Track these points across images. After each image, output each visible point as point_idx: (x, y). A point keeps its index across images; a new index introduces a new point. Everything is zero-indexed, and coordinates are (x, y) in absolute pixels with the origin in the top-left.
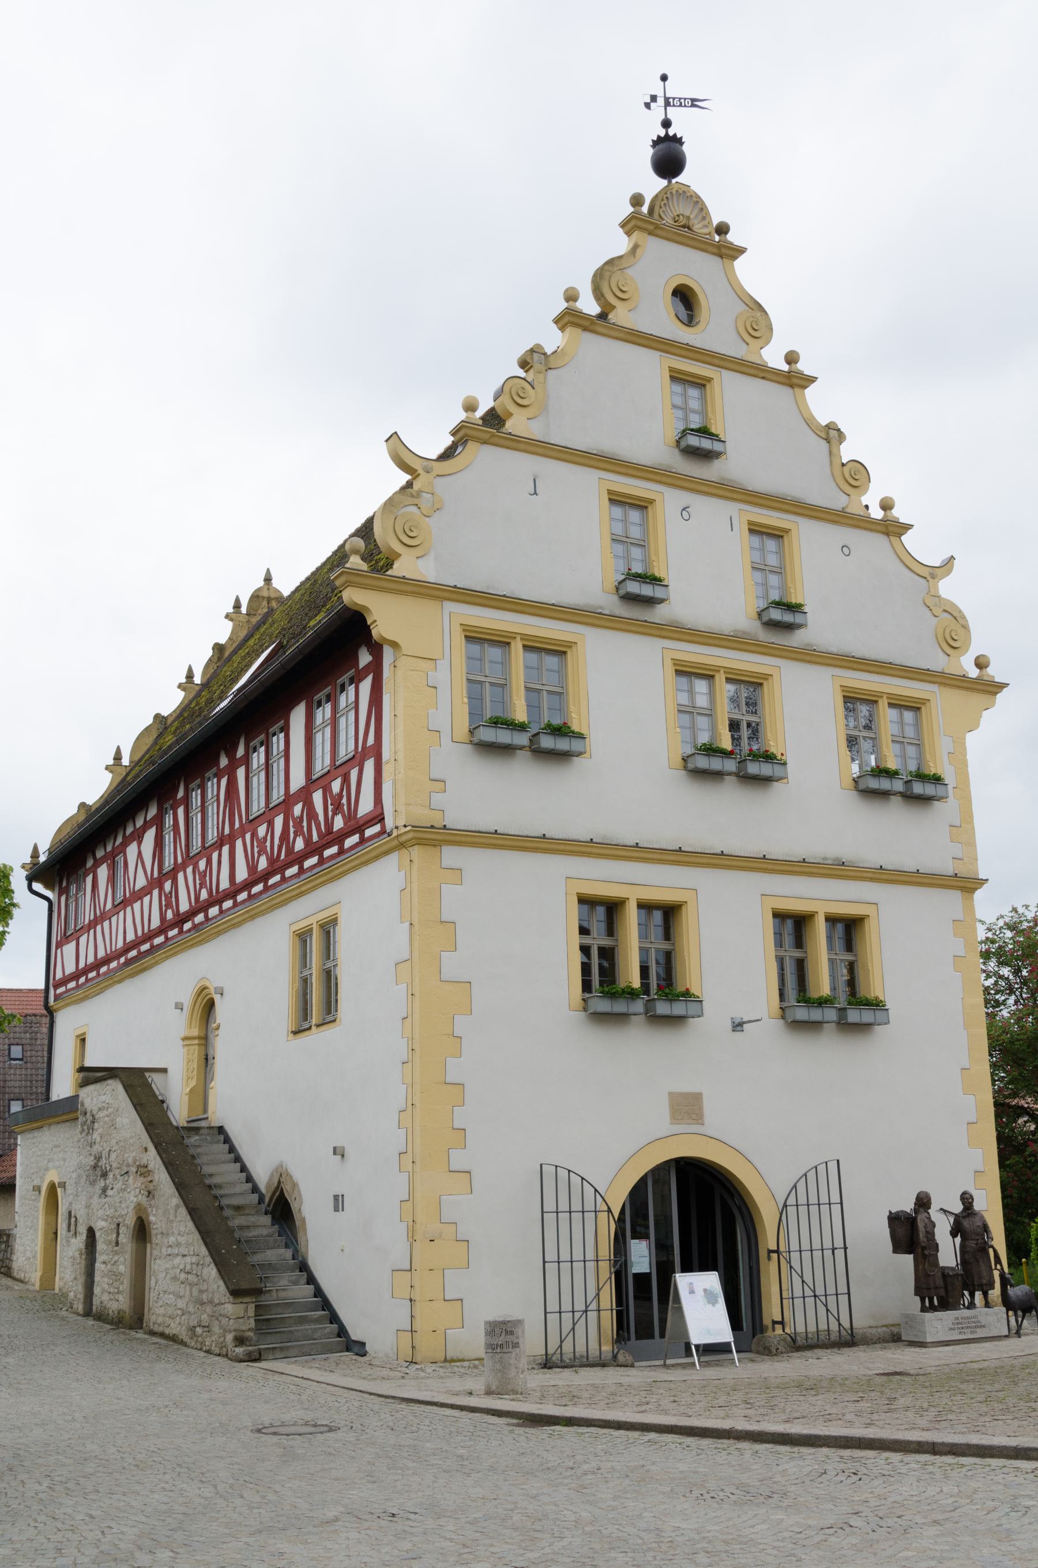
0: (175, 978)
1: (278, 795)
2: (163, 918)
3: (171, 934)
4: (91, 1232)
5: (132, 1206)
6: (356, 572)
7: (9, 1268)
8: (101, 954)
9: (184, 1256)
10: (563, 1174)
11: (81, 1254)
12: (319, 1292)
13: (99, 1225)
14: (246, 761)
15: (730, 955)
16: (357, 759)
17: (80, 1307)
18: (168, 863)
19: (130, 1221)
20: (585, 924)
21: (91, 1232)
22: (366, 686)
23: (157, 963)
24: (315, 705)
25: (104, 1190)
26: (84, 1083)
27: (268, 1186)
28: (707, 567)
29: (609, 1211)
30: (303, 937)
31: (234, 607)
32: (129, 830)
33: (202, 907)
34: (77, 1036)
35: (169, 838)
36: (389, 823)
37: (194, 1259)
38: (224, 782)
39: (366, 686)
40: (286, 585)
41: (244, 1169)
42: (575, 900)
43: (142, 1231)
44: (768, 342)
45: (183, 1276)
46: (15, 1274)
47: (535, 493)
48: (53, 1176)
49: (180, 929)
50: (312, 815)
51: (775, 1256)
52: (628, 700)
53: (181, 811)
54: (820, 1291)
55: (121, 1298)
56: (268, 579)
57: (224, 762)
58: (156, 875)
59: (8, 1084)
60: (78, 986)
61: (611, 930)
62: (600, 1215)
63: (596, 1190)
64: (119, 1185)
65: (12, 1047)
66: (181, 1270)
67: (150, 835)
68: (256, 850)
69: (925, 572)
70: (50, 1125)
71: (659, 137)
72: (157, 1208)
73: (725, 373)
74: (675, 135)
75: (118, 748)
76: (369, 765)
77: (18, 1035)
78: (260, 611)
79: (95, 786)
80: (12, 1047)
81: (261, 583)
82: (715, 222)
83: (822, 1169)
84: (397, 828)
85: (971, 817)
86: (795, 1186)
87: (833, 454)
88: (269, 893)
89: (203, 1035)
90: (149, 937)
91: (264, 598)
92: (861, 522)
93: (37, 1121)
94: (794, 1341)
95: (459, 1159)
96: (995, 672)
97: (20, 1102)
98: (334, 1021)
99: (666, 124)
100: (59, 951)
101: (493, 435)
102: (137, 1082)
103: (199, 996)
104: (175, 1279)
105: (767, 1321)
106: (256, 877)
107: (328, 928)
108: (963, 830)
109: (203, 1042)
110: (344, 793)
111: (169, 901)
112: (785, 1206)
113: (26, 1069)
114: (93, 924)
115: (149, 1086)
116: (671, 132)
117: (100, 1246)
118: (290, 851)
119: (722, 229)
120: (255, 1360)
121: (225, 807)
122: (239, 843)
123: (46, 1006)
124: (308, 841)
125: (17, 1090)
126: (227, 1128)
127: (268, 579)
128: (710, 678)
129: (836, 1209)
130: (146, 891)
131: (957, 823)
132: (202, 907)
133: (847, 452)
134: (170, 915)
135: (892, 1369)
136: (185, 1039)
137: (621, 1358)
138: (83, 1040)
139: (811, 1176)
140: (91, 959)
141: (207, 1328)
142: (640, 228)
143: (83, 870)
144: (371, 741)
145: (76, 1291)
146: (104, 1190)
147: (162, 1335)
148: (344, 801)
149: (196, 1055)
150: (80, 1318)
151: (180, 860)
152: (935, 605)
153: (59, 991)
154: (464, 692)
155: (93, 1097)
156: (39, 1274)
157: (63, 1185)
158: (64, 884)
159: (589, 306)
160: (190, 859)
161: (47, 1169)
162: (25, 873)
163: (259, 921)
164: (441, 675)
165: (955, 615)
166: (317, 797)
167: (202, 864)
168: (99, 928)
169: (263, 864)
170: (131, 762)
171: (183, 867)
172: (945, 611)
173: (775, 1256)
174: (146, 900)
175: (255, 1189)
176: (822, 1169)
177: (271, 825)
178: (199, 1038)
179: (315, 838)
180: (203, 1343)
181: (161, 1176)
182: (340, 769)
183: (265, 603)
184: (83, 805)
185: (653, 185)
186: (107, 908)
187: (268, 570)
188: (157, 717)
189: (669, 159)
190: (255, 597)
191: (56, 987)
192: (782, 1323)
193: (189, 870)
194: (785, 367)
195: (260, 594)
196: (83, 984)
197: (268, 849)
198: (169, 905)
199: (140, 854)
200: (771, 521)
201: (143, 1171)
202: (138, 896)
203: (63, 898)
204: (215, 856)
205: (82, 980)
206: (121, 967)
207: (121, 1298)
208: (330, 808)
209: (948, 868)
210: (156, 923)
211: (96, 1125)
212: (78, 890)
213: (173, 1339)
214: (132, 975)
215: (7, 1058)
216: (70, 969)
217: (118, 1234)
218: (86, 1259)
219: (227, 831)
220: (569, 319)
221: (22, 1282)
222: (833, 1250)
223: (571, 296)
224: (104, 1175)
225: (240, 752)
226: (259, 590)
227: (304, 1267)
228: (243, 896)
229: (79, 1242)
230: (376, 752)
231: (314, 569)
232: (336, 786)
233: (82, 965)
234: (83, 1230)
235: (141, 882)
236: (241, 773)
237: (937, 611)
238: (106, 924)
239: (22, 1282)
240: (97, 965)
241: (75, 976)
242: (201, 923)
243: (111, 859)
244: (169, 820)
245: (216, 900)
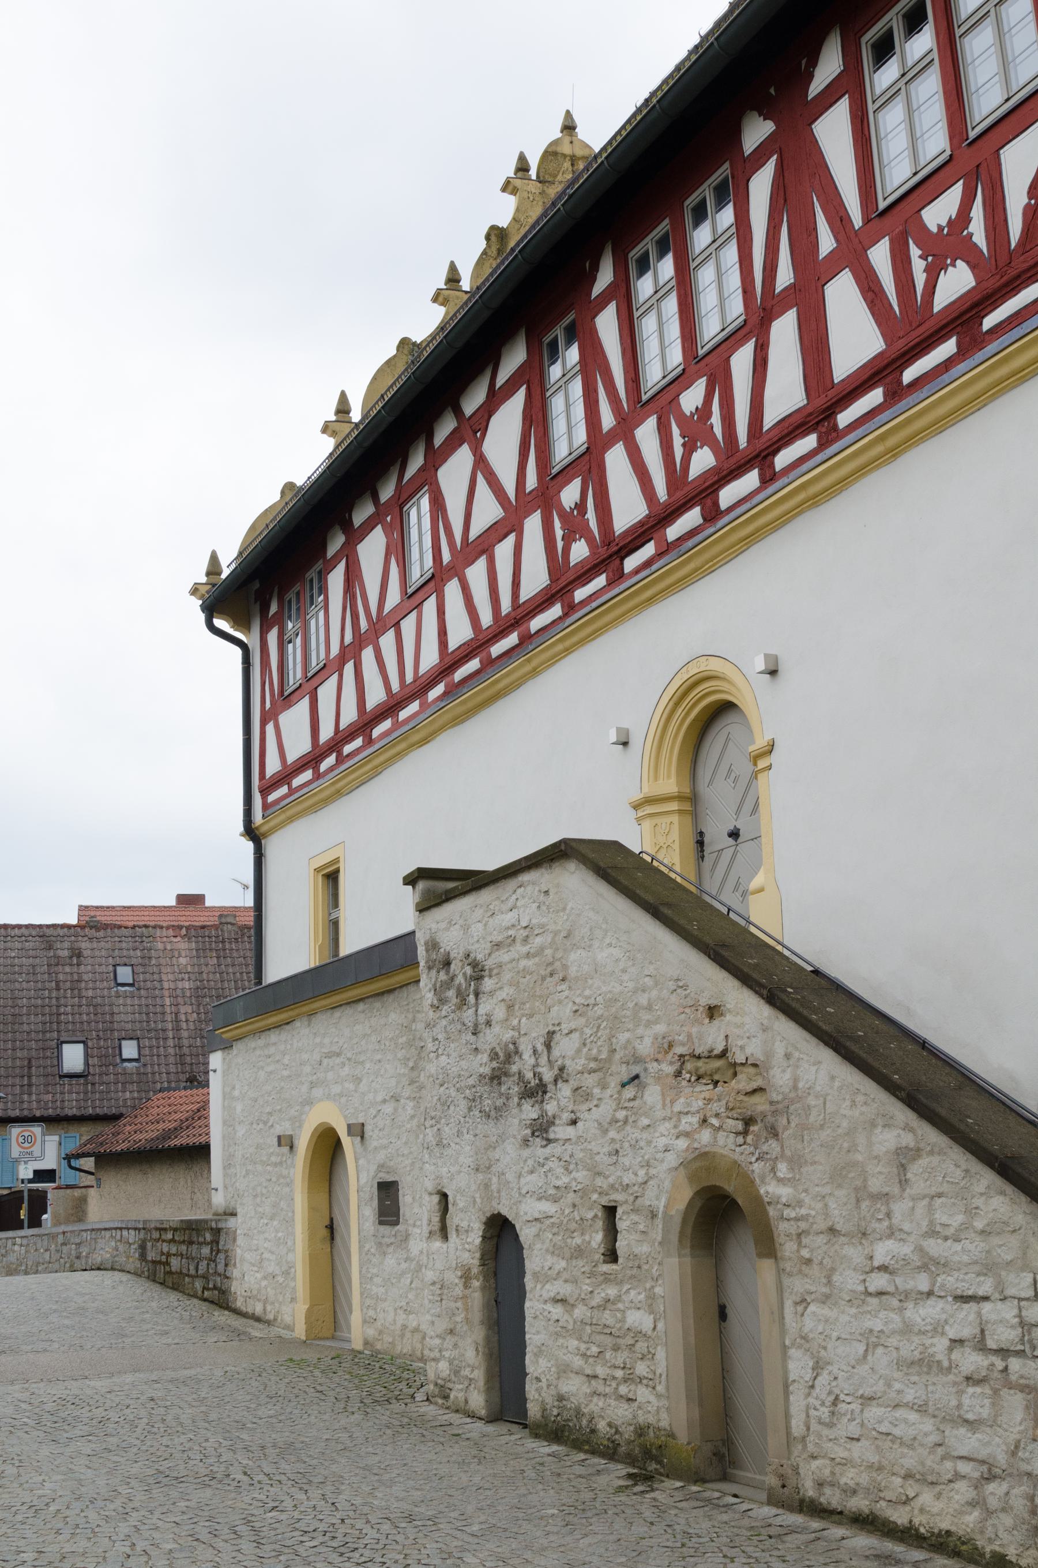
4: (500, 1231)
7: (224, 1292)
11: (466, 1277)
13: (526, 1213)
21: (500, 1231)
23: (534, 673)
25: (541, 1129)
34: (317, 870)
40: (598, 133)
46: (239, 1304)
48: (329, 1113)
55: (643, 1393)
56: (569, 127)
59: (117, 1018)
65: (119, 969)
70: (311, 1014)
72: (796, 1162)
75: (343, 394)
77: (125, 953)
78: (559, 178)
80: (119, 969)
81: (557, 134)
89: (687, 790)
91: (565, 156)
93: (279, 1009)
97: (134, 1043)
100: (270, 728)
103: (677, 704)
109: (687, 806)
113: (140, 997)
123: (251, 832)
125: (129, 1026)
127: (569, 127)
130: (510, 525)
138: (332, 877)
140: (350, 715)
143: (319, 565)
145: (459, 1357)
146: (541, 1129)
149: (675, 835)
150: (480, 1424)
153: (271, 798)
156: (302, 1308)
157: (358, 1131)
161: (309, 1102)
163: (1026, 384)
178: (680, 798)
183: (567, 164)
184: (289, 486)
186: (388, 607)
188: (404, 342)
190: (550, 154)
191: (265, 791)
195: (559, 149)
201: (714, 1067)
203: (273, 637)
211: (488, 984)
214: (458, 720)
215: (112, 984)
218: (483, 1288)
221: (258, 1320)
226: (556, 143)
231: (647, 95)
233: (326, 733)
235: (487, 511)
238: (387, 641)
239: (258, 1320)
241: (311, 761)
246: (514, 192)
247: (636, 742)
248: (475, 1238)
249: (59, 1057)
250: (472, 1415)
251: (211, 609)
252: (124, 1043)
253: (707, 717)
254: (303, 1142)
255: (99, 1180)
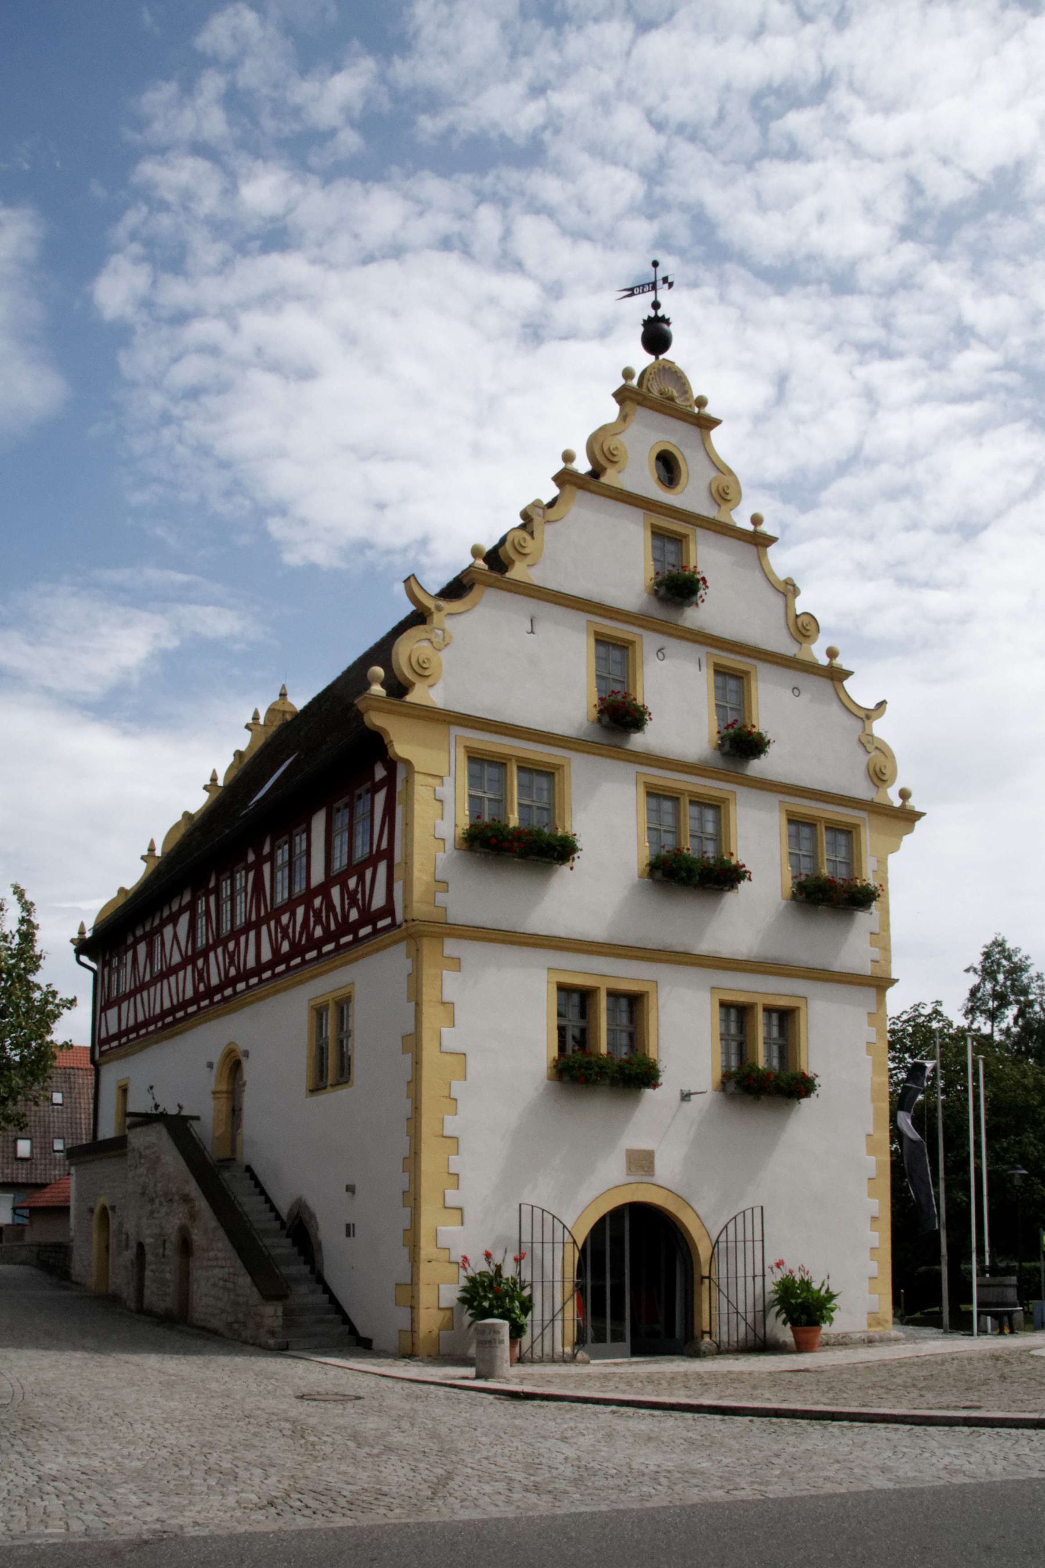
0: (207, 1041)
1: (299, 888)
2: (195, 989)
3: (203, 1004)
4: (141, 1246)
5: (176, 1227)
6: (376, 698)
8: (141, 1018)
9: (223, 1267)
10: (538, 1213)
11: (132, 1264)
12: (333, 1300)
13: (148, 1241)
14: (271, 857)
15: (686, 1036)
16: (372, 861)
17: (132, 1305)
18: (201, 942)
19: (174, 1238)
20: (562, 1010)
21: (141, 1246)
22: (380, 798)
24: (334, 811)
25: (152, 1212)
26: (132, 1126)
27: (289, 1214)
28: (680, 709)
29: (574, 1242)
30: (319, 1012)
31: (254, 719)
32: (166, 913)
33: (232, 982)
34: (120, 1087)
35: (201, 923)
36: (399, 917)
37: (231, 1270)
38: (251, 875)
39: (380, 798)
40: (299, 702)
41: (268, 1200)
42: (554, 988)
43: (186, 1247)
44: (738, 504)
45: (221, 1283)
47: (532, 632)
48: (103, 1200)
49: (211, 1001)
50: (330, 907)
51: (707, 1281)
52: (609, 821)
53: (212, 899)
54: (741, 1309)
56: (283, 695)
57: (251, 857)
58: (190, 953)
60: (120, 1045)
61: (583, 1014)
62: (567, 1246)
63: (564, 1226)
64: (164, 1210)
66: (218, 1276)
67: (184, 920)
68: (279, 935)
69: (862, 714)
71: (649, 317)
73: (699, 531)
74: (663, 316)
76: (382, 867)
79: (132, 874)
81: (277, 698)
82: (695, 395)
83: (749, 1213)
84: (406, 921)
85: (888, 925)
86: (726, 1227)
87: (788, 606)
88: (291, 973)
90: (184, 1005)
92: (810, 668)
94: (719, 1346)
95: (453, 1197)
96: (915, 803)
98: (347, 1082)
99: (656, 305)
101: (498, 580)
102: (178, 1126)
104: (214, 1285)
105: (697, 1333)
106: (278, 958)
107: (343, 1005)
108: (881, 938)
110: (360, 889)
111: (201, 976)
112: (717, 1242)
114: (133, 993)
115: (188, 1130)
116: (660, 313)
117: (149, 1257)
118: (310, 936)
119: (701, 402)
120: (283, 1350)
121: (252, 897)
122: (264, 929)
123: (93, 1061)
124: (326, 928)
126: (253, 1167)
127: (283, 695)
128: (675, 800)
129: (758, 1245)
130: (181, 966)
131: (877, 930)
132: (230, 981)
133: (801, 605)
134: (202, 987)
135: (796, 1368)
136: (214, 1093)
137: (579, 1356)
139: (740, 1219)
141: (244, 1324)
142: (631, 399)
144: (384, 845)
145: (128, 1292)
146: (152, 1212)
147: (203, 1328)
148: (359, 896)
151: (211, 941)
152: (869, 742)
154: (466, 805)
155: (138, 1139)
157: (113, 1208)
158: (107, 958)
159: (582, 465)
160: (220, 941)
162: (73, 947)
164: (446, 791)
165: (883, 750)
166: (335, 892)
167: (231, 946)
168: (138, 997)
169: (285, 947)
170: (163, 853)
171: (213, 947)
172: (877, 748)
173: (707, 1281)
174: (181, 974)
175: (278, 1217)
176: (749, 1213)
177: (293, 915)
178: (226, 1092)
179: (333, 927)
180: (240, 1335)
181: (202, 1204)
182: (357, 869)
183: (281, 715)
185: (642, 360)
187: (924, 814)
189: (656, 336)
190: (271, 711)
191: (101, 1046)
192: (710, 1333)
193: (220, 950)
194: (750, 527)
196: (125, 1043)
197: (291, 935)
198: (201, 979)
199: (175, 936)
200: (734, 669)
201: (186, 1199)
202: (173, 970)
203: (106, 970)
204: (243, 939)
205: (124, 1040)
206: (157, 1030)
207: (168, 1298)
208: (347, 902)
209: (867, 970)
210: (189, 993)
212: (120, 962)
213: (215, 1333)
216: (113, 1030)
217: (164, 1249)
219: (254, 918)
220: (564, 478)
222: (754, 1277)
223: (568, 457)
224: (152, 1201)
225: (267, 849)
226: (275, 703)
227: (320, 1280)
228: (267, 975)
229: (130, 1254)
230: (388, 855)
232: (352, 883)
233: (123, 1027)
234: (133, 1244)
235: (176, 959)
236: (267, 868)
237: (870, 748)
238: (145, 993)
240: (137, 1027)
241: (117, 1036)
242: (230, 996)
243: (149, 938)
244: (201, 907)
245: (244, 975)
246: (250, 730)
247: (215, 1066)
248: (134, 1250)
249: (58, 1092)
250: (131, 1311)
251: (78, 952)
252: (56, 1141)
253: (234, 1066)
254: (97, 1210)
255: (31, 1222)
